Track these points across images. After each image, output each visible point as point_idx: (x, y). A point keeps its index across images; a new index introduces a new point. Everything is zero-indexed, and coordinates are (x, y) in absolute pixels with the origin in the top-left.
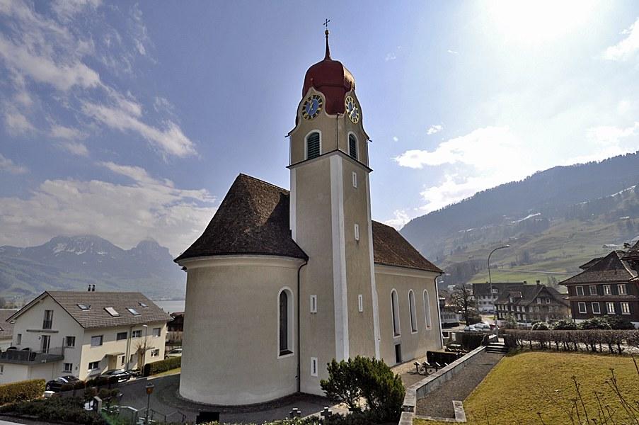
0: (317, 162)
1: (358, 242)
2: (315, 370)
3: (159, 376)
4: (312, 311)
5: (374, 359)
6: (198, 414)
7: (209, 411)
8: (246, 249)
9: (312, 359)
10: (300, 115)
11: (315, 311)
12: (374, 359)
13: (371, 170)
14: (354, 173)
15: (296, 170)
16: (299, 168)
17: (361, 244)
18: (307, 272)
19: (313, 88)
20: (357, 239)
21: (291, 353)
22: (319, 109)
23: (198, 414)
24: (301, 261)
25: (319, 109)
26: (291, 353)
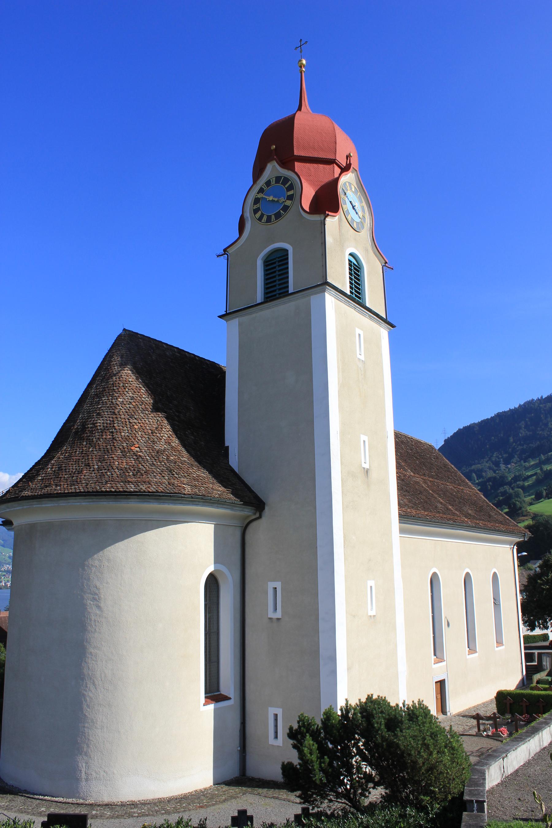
0: (282, 308)
1: (367, 471)
2: (276, 732)
3: (402, 667)
4: (271, 615)
5: (451, 728)
6: (46, 819)
7: (62, 812)
8: (136, 483)
9: (272, 711)
10: (248, 214)
11: (279, 615)
12: (451, 728)
13: (331, 706)
14: (358, 331)
15: (240, 324)
16: (246, 318)
17: (374, 475)
18: (261, 533)
19: (275, 163)
20: (366, 466)
21: (230, 699)
22: (288, 203)
23: (46, 819)
24: (247, 512)
25: (288, 203)
26: (230, 699)
